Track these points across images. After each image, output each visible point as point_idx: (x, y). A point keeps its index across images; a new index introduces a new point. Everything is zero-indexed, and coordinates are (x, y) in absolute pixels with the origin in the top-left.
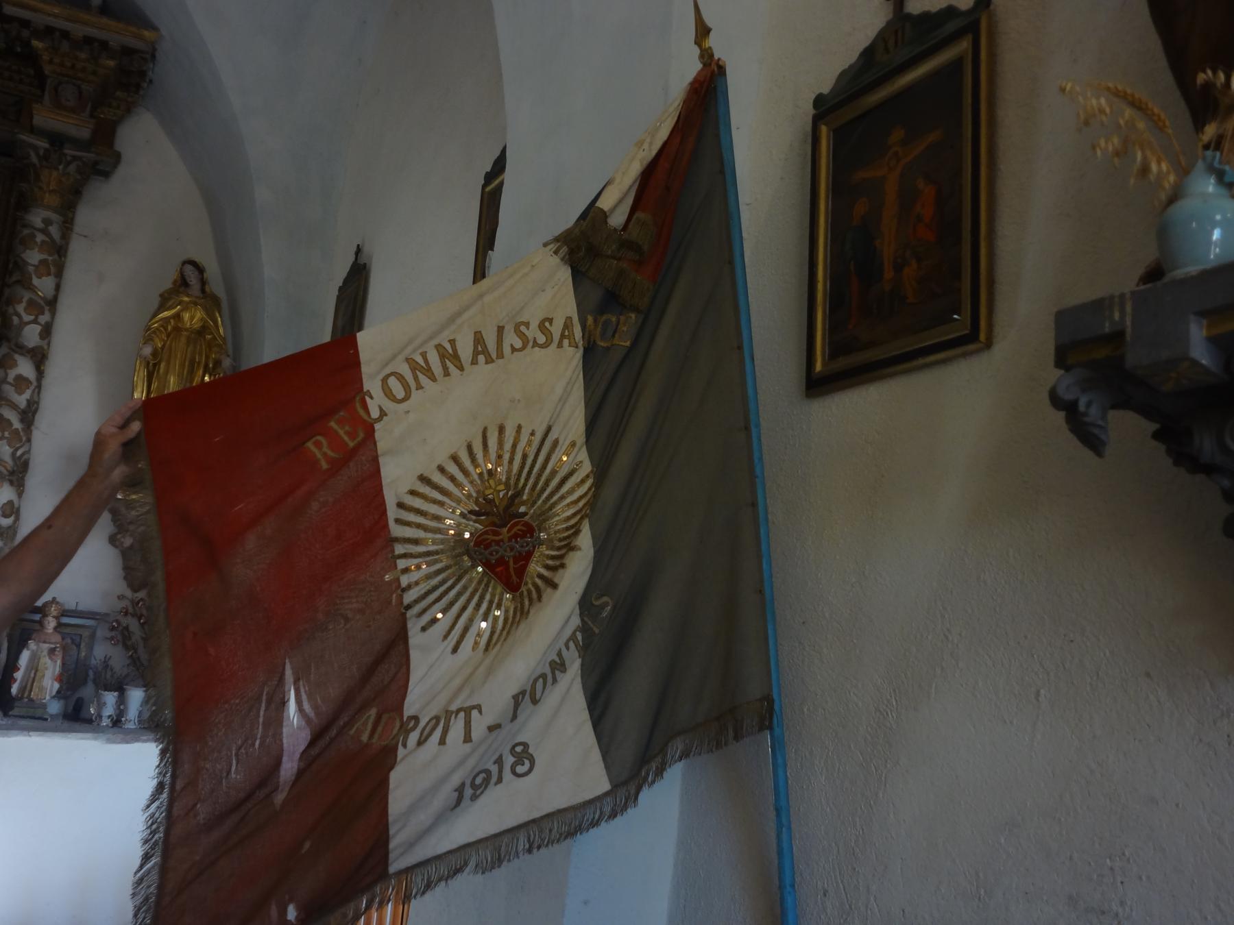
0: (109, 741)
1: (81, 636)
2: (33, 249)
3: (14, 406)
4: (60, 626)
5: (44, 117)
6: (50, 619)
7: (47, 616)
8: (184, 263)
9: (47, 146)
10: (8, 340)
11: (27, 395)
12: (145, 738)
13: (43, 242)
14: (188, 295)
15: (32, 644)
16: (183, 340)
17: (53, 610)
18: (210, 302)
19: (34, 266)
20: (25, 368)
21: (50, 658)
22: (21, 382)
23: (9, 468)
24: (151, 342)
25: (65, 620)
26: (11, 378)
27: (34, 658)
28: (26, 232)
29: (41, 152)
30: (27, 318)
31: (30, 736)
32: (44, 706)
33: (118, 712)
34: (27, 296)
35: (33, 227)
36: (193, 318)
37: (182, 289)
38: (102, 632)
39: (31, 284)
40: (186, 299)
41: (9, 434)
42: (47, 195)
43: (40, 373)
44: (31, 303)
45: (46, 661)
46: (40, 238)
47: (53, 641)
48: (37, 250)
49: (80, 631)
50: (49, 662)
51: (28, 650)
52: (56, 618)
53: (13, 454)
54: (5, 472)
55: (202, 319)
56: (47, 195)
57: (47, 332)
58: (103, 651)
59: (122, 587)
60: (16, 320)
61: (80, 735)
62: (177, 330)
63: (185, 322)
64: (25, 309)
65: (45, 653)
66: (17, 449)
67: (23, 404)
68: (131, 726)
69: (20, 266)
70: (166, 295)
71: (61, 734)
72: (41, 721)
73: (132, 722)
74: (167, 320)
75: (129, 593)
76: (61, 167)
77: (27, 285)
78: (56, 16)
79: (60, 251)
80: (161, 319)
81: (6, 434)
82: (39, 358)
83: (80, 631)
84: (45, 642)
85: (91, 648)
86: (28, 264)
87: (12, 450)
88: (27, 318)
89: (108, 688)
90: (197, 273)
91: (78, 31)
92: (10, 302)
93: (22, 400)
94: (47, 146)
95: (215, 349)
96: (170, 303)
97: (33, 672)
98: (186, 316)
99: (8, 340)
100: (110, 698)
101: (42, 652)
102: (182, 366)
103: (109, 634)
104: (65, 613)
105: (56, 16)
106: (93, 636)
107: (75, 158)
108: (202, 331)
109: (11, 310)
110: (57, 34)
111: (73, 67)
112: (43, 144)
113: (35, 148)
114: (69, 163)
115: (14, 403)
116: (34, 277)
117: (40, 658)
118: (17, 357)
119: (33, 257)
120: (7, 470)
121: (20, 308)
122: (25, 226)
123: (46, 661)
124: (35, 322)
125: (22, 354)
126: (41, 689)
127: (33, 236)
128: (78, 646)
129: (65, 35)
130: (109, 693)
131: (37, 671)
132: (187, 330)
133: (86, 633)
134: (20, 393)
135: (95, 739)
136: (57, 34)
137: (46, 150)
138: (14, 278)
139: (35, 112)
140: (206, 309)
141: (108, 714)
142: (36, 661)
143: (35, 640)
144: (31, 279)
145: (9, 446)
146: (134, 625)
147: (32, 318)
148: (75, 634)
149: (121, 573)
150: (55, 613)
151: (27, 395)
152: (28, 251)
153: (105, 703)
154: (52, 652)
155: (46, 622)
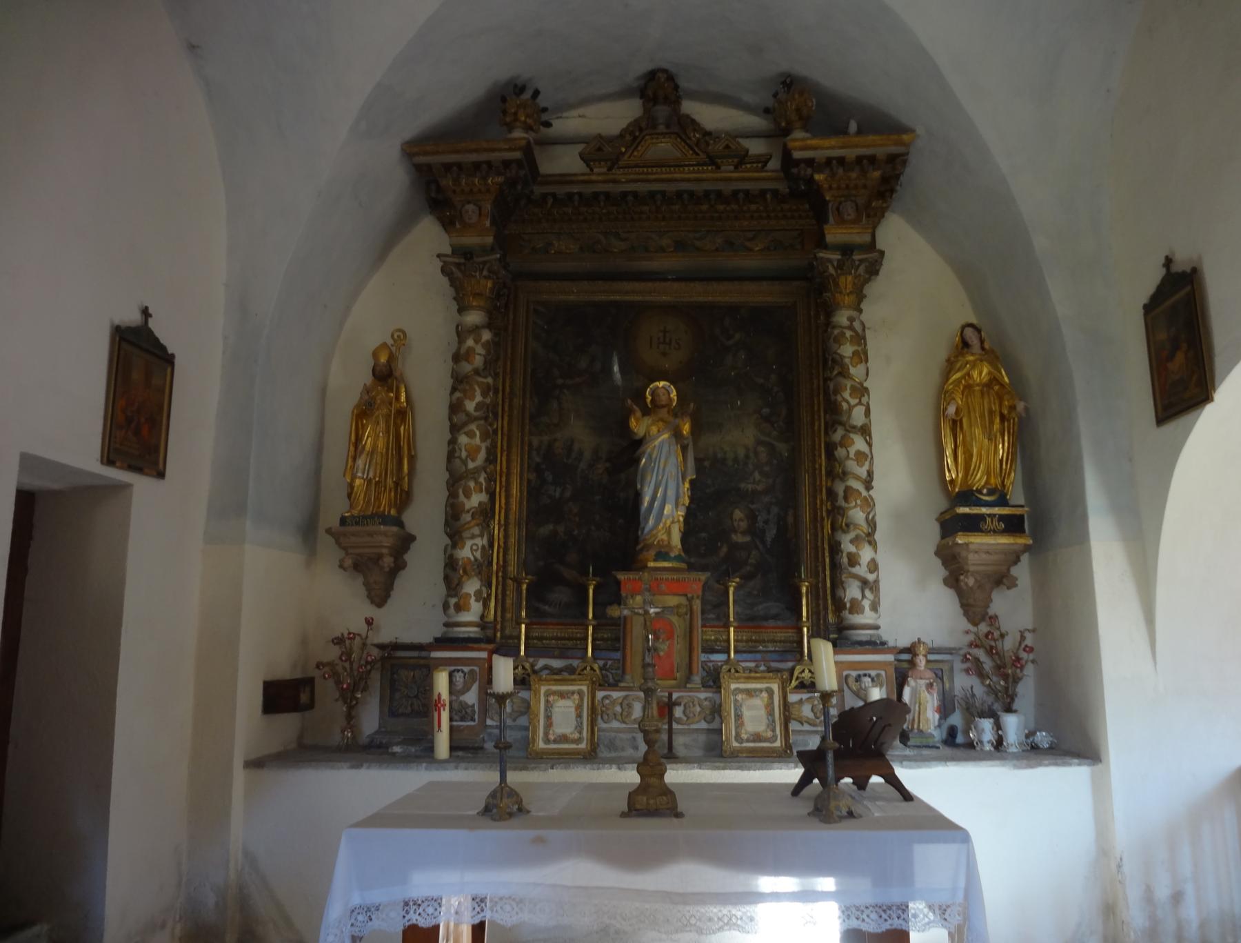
0: (1016, 767)
1: (942, 670)
2: (846, 344)
3: (857, 478)
4: (928, 661)
5: (834, 234)
6: (921, 657)
7: (918, 655)
8: (963, 328)
9: (839, 257)
10: (841, 423)
11: (866, 467)
12: (1046, 762)
13: (851, 336)
14: (973, 354)
15: (911, 681)
16: (978, 395)
17: (922, 650)
18: (991, 355)
19: (849, 357)
20: (859, 444)
21: (928, 692)
22: (861, 457)
23: (865, 531)
24: (953, 401)
25: (931, 657)
26: (852, 455)
27: (915, 693)
28: (836, 332)
29: (835, 264)
30: (853, 401)
31: (947, 766)
32: (932, 736)
33: (996, 737)
34: (849, 384)
35: (841, 327)
36: (982, 373)
37: (966, 350)
38: (958, 666)
39: (849, 373)
40: (971, 358)
41: (861, 501)
42: (846, 297)
43: (870, 445)
44: (854, 389)
45: (925, 695)
46: (848, 334)
47: (927, 676)
48: (848, 344)
49: (940, 666)
50: (928, 695)
51: (908, 686)
52: (925, 656)
53: (867, 518)
54: (864, 535)
55: (989, 373)
56: (846, 297)
57: (868, 413)
58: (963, 682)
59: (964, 624)
60: (845, 405)
61: (989, 763)
62: (968, 387)
63: (975, 379)
64: (851, 395)
65: (924, 688)
66: (869, 514)
67: (864, 475)
68: (1013, 750)
69: (838, 361)
70: (952, 359)
71: (973, 763)
72: (934, 750)
73: (1014, 746)
74: (958, 381)
75: (970, 627)
76: (853, 272)
77: (844, 374)
78: (833, 148)
79: (860, 339)
80: (954, 381)
81: (859, 502)
82: (865, 431)
83: (940, 666)
84: (921, 678)
85: (952, 680)
86: (845, 357)
87: (864, 515)
88: (853, 401)
89: (982, 715)
90: (976, 333)
91: (850, 154)
92: (837, 391)
93: (862, 472)
94: (839, 257)
95: (1006, 397)
96: (958, 365)
97: (917, 706)
98: (975, 374)
99: (841, 423)
100: (987, 724)
101: (921, 687)
102: (982, 416)
103: (965, 666)
104: (932, 651)
105: (833, 148)
106: (951, 670)
107: (861, 261)
108: (994, 381)
109: (839, 398)
110: (834, 162)
111: (847, 187)
112: (836, 257)
113: (830, 261)
114: (859, 266)
115: (858, 476)
116: (850, 367)
117: (920, 694)
118: (852, 435)
119: (847, 350)
120: (864, 533)
121: (846, 395)
122: (834, 327)
123: (925, 695)
124: (860, 403)
125: (855, 433)
126: (927, 720)
127: (843, 334)
128: (942, 679)
129: (841, 161)
130: (986, 720)
131: (920, 704)
132: (978, 385)
133: (945, 667)
134: (861, 466)
135: (1003, 766)
136: (834, 162)
137: (839, 261)
138: (835, 372)
139: (826, 232)
140: (991, 363)
141: (988, 739)
142: (917, 696)
143: (912, 677)
144: (849, 369)
145: (862, 511)
146: (981, 654)
147: (857, 401)
148: (937, 669)
149: (960, 611)
150: (923, 652)
151: (866, 467)
152: (842, 347)
153: (983, 730)
154: (930, 686)
155: (918, 661)
